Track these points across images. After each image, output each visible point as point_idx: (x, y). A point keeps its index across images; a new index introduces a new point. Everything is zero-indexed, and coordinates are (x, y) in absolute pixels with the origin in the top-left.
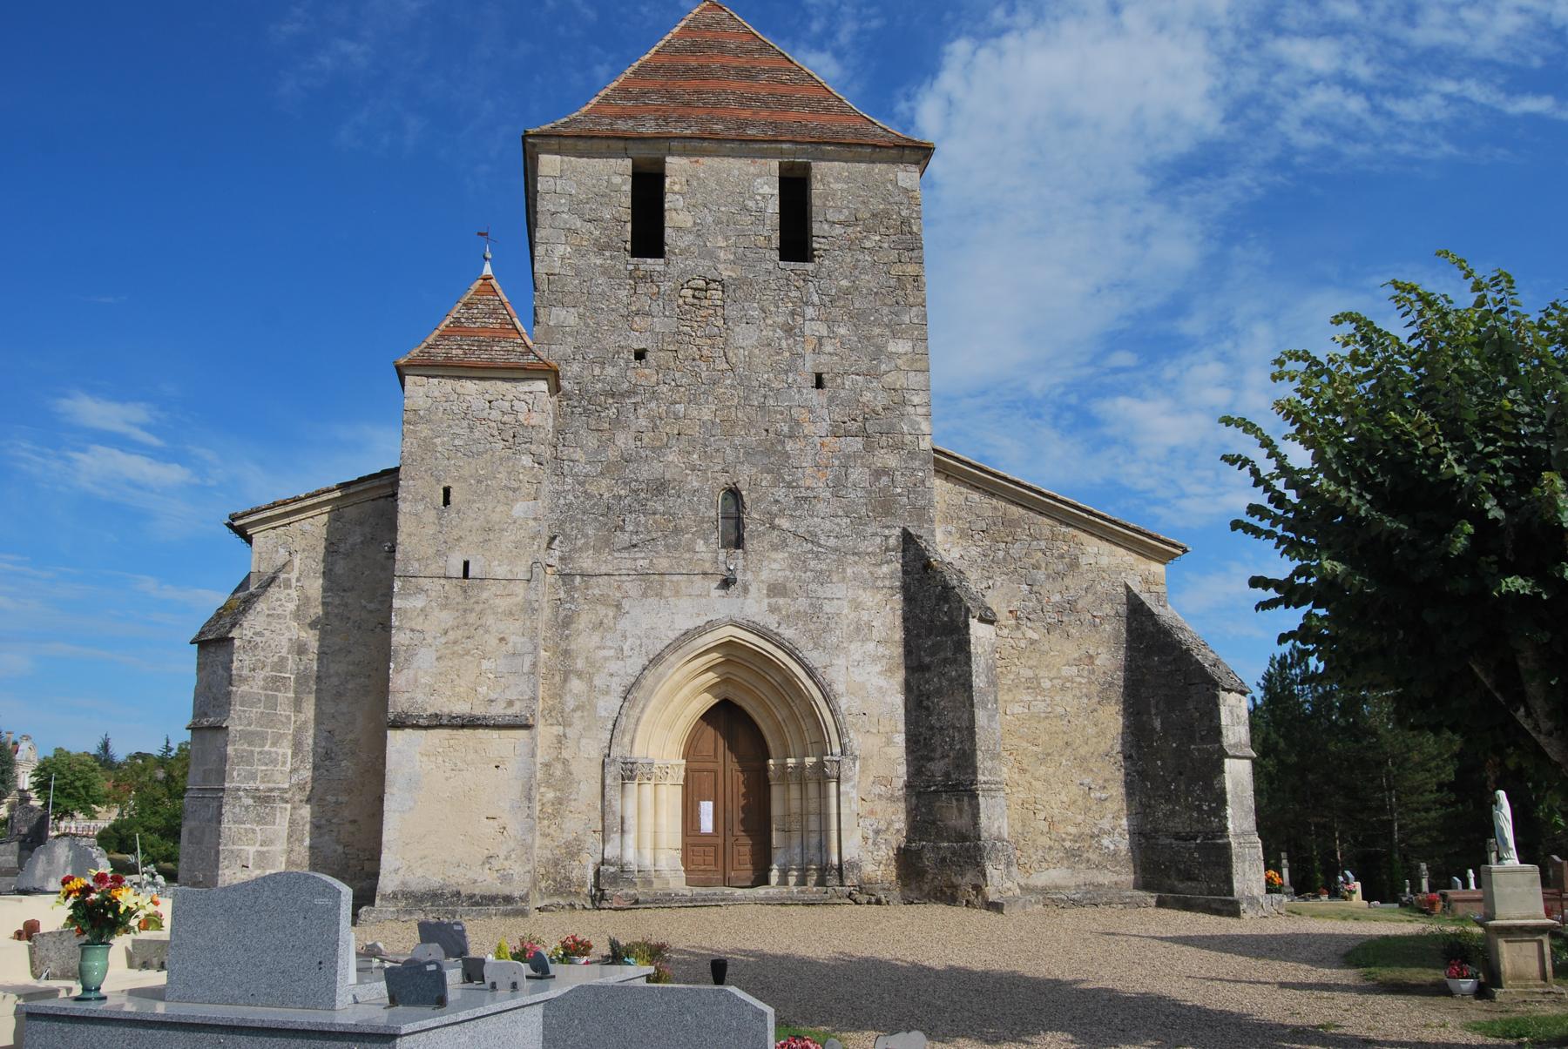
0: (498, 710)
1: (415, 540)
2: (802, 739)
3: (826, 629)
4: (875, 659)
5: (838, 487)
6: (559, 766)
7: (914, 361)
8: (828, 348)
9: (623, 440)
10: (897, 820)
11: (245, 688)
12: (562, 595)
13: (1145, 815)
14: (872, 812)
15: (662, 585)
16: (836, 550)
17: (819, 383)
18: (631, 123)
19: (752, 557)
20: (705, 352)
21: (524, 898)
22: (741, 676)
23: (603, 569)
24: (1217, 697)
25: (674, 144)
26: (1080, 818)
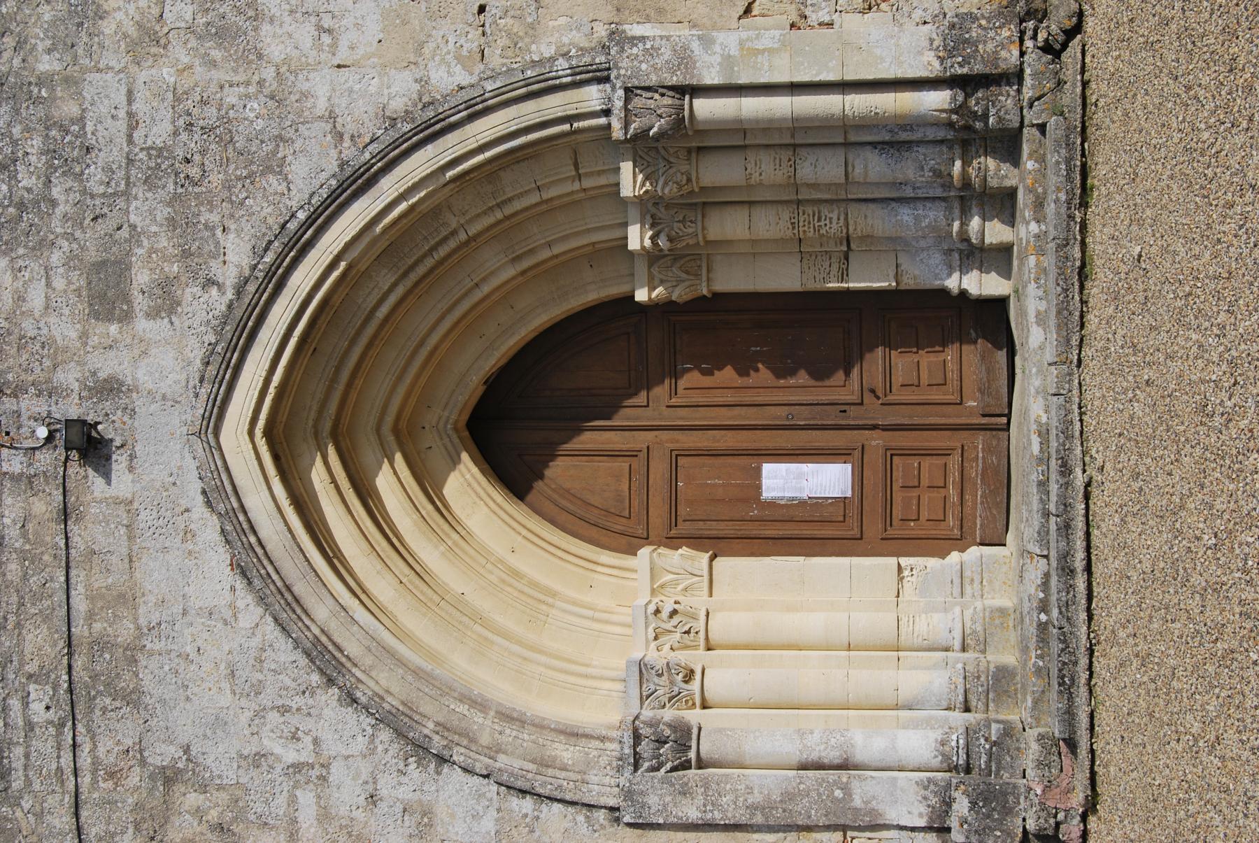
2: (570, 205)
3: (222, 132)
15: (101, 644)
22: (383, 392)
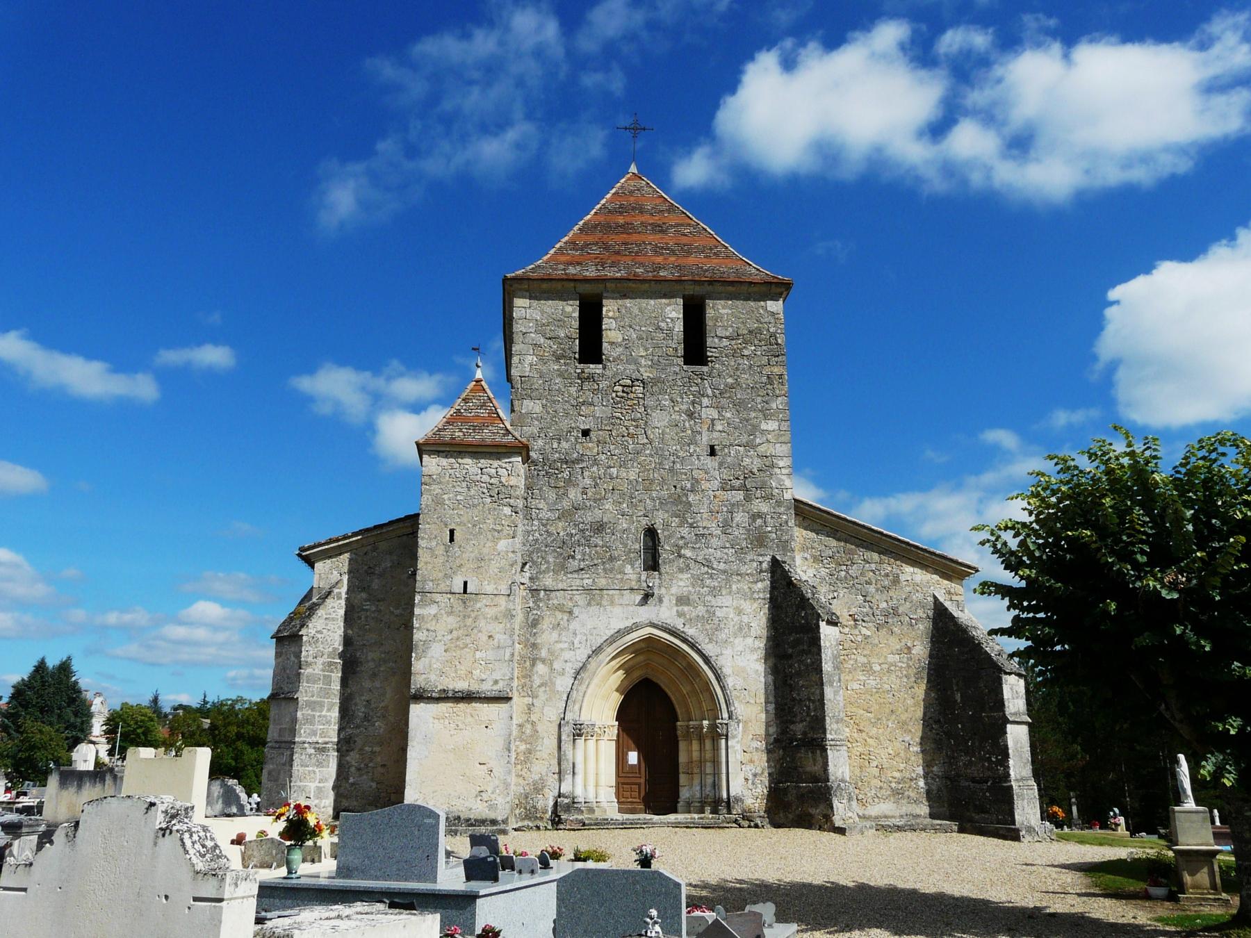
0: (487, 688)
1: (430, 567)
4: (753, 650)
5: (726, 526)
6: (529, 726)
9: (574, 494)
11: (309, 670)
12: (531, 605)
13: (951, 764)
14: (751, 761)
16: (725, 572)
17: (713, 452)
18: (578, 268)
19: (665, 577)
21: (505, 822)
23: (560, 586)
24: (1000, 679)
26: (902, 766)
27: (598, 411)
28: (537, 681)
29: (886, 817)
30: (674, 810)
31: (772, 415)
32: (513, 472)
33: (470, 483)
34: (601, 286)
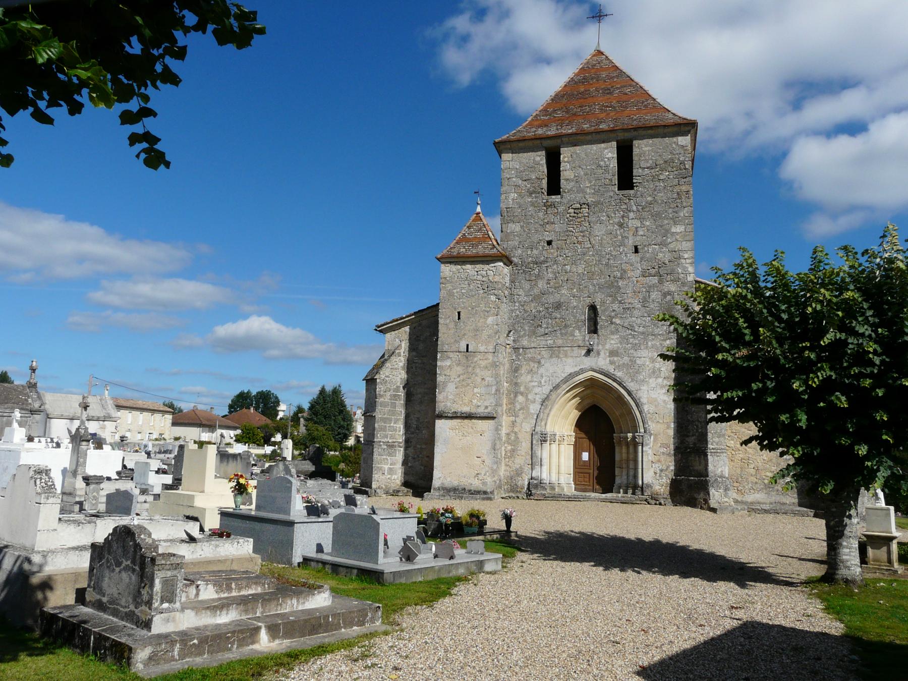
0: (481, 411)
1: (446, 336)
3: (638, 372)
4: (662, 387)
5: (645, 302)
7: (685, 236)
8: (641, 233)
9: (541, 284)
10: (670, 464)
11: (382, 399)
14: (659, 461)
16: (643, 333)
17: (636, 251)
18: (545, 129)
19: (601, 337)
20: (580, 239)
21: (492, 493)
23: (533, 345)
25: (565, 139)
27: (557, 227)
28: (518, 407)
29: (759, 503)
30: (610, 491)
31: (680, 221)
32: (500, 272)
33: (469, 280)
34: (559, 141)
